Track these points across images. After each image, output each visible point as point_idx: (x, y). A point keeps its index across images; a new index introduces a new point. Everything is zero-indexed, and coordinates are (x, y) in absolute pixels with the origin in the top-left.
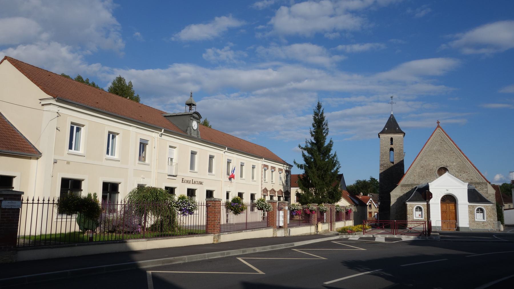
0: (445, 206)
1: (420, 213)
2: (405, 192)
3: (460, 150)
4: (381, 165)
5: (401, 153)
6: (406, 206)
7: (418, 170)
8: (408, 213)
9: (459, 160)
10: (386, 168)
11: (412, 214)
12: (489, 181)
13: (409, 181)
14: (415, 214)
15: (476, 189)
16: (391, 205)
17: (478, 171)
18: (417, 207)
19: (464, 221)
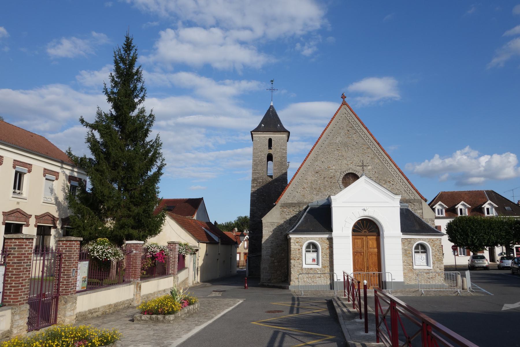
0: (359, 241)
1: (314, 255)
2: (288, 217)
3: (378, 144)
4: (254, 180)
5: (284, 164)
6: (287, 241)
7: (310, 178)
8: (292, 256)
9: (377, 161)
10: (262, 185)
11: (300, 259)
12: (425, 197)
13: (294, 197)
14: (305, 261)
15: (410, 209)
16: (264, 240)
17: (407, 180)
18: (310, 244)
19: (394, 270)
